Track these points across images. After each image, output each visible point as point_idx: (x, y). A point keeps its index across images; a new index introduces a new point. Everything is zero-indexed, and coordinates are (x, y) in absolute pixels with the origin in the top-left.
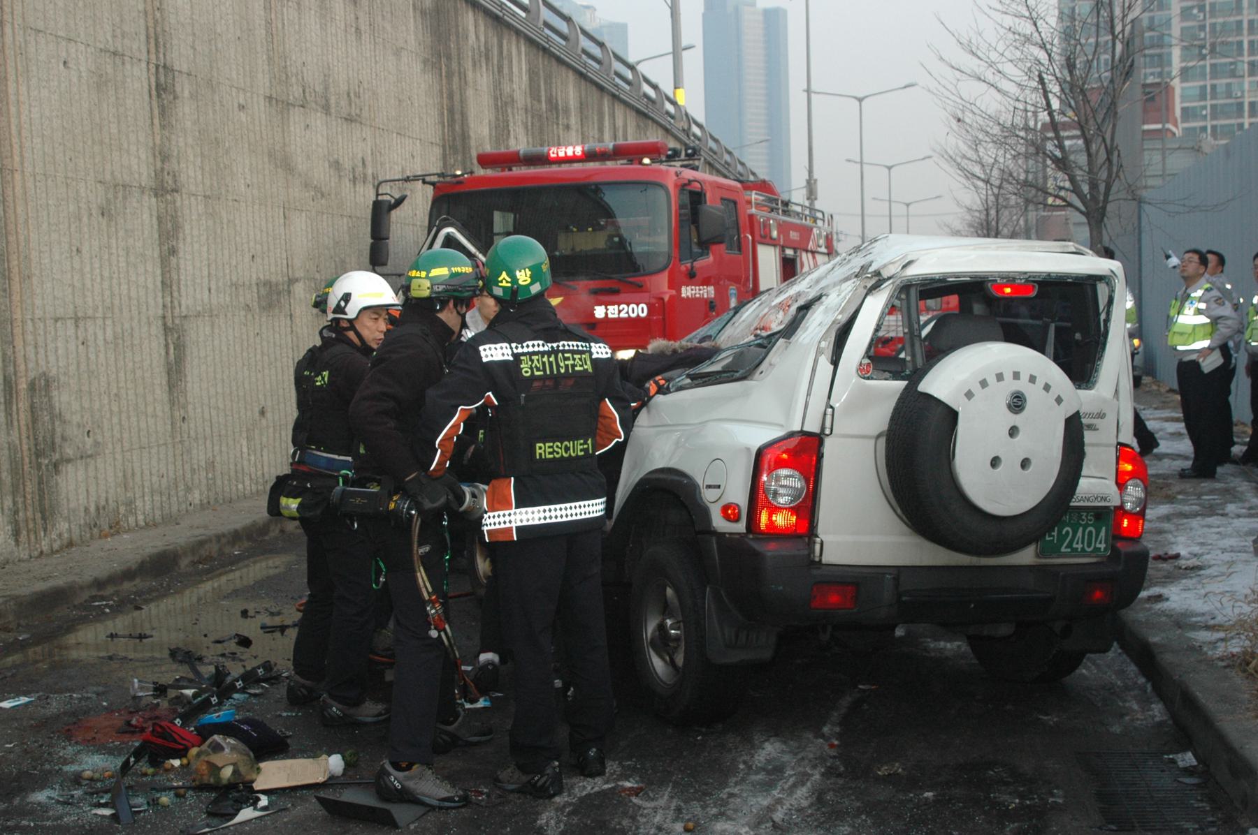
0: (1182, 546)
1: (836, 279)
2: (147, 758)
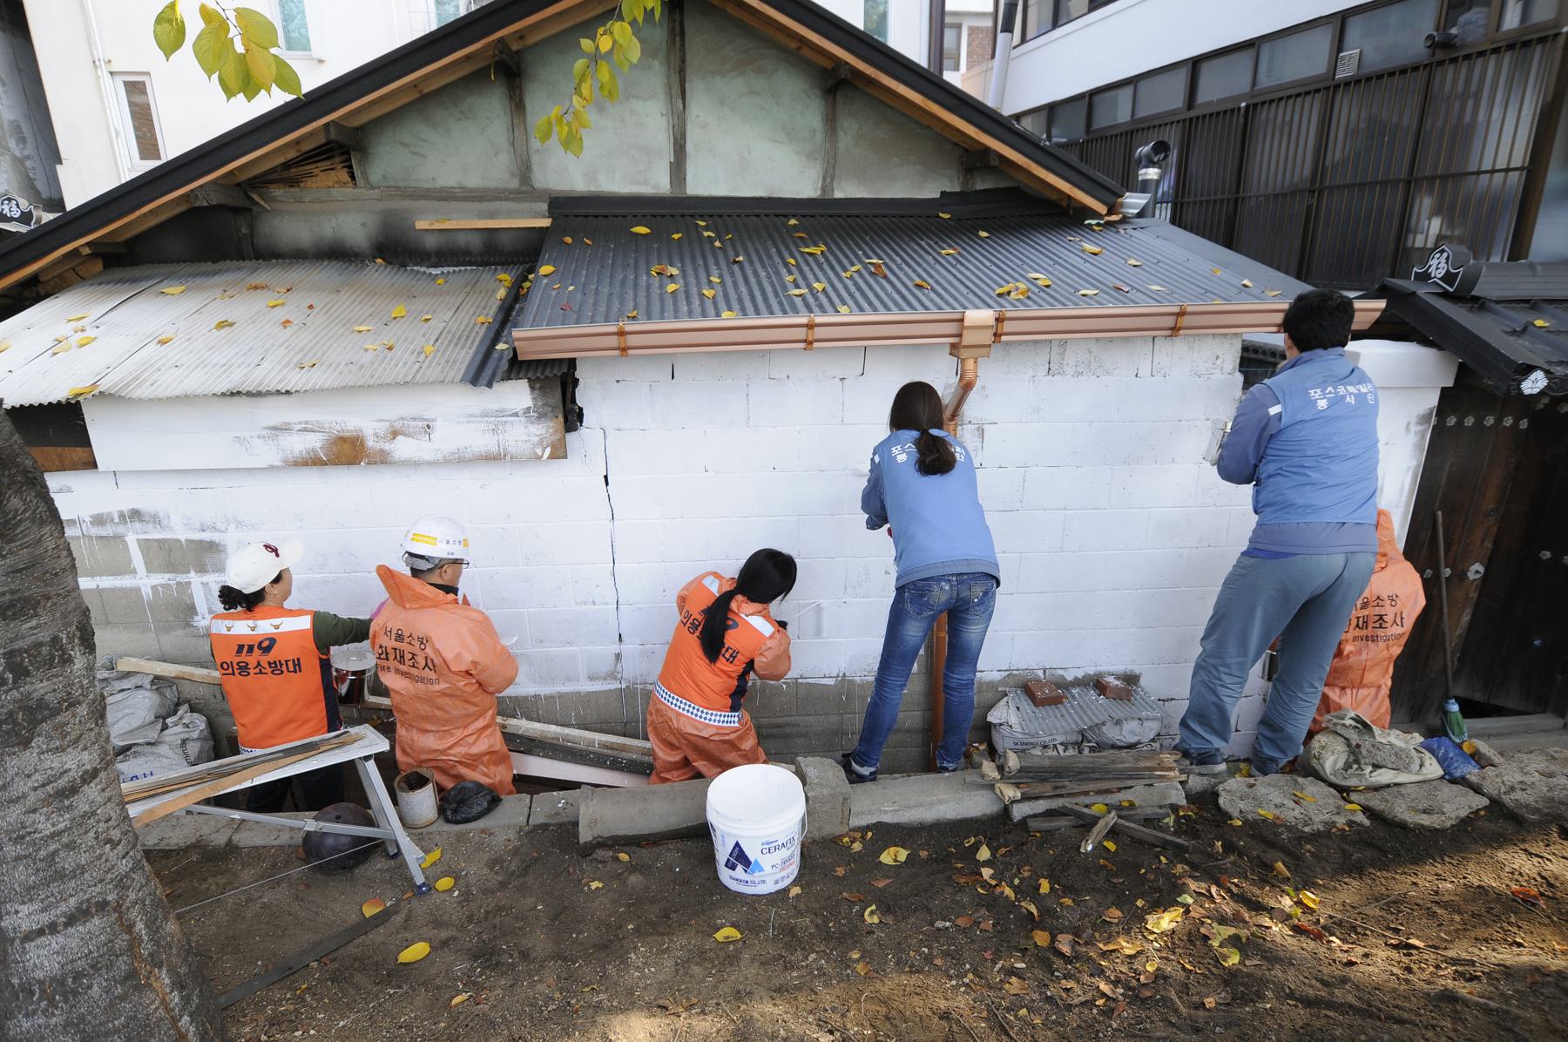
1: (135, 725)
2: (1305, 288)
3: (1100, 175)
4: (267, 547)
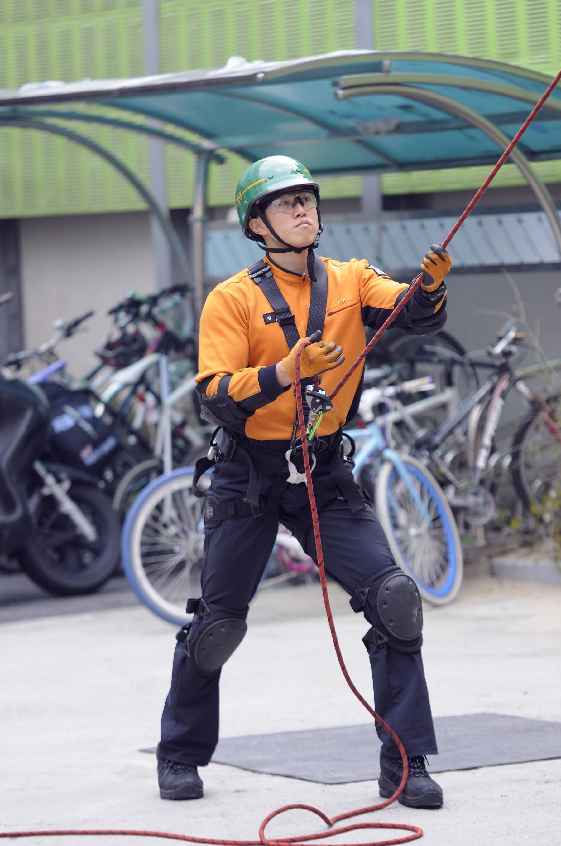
0: (309, 341)
3: (403, 299)
4: (429, 268)
